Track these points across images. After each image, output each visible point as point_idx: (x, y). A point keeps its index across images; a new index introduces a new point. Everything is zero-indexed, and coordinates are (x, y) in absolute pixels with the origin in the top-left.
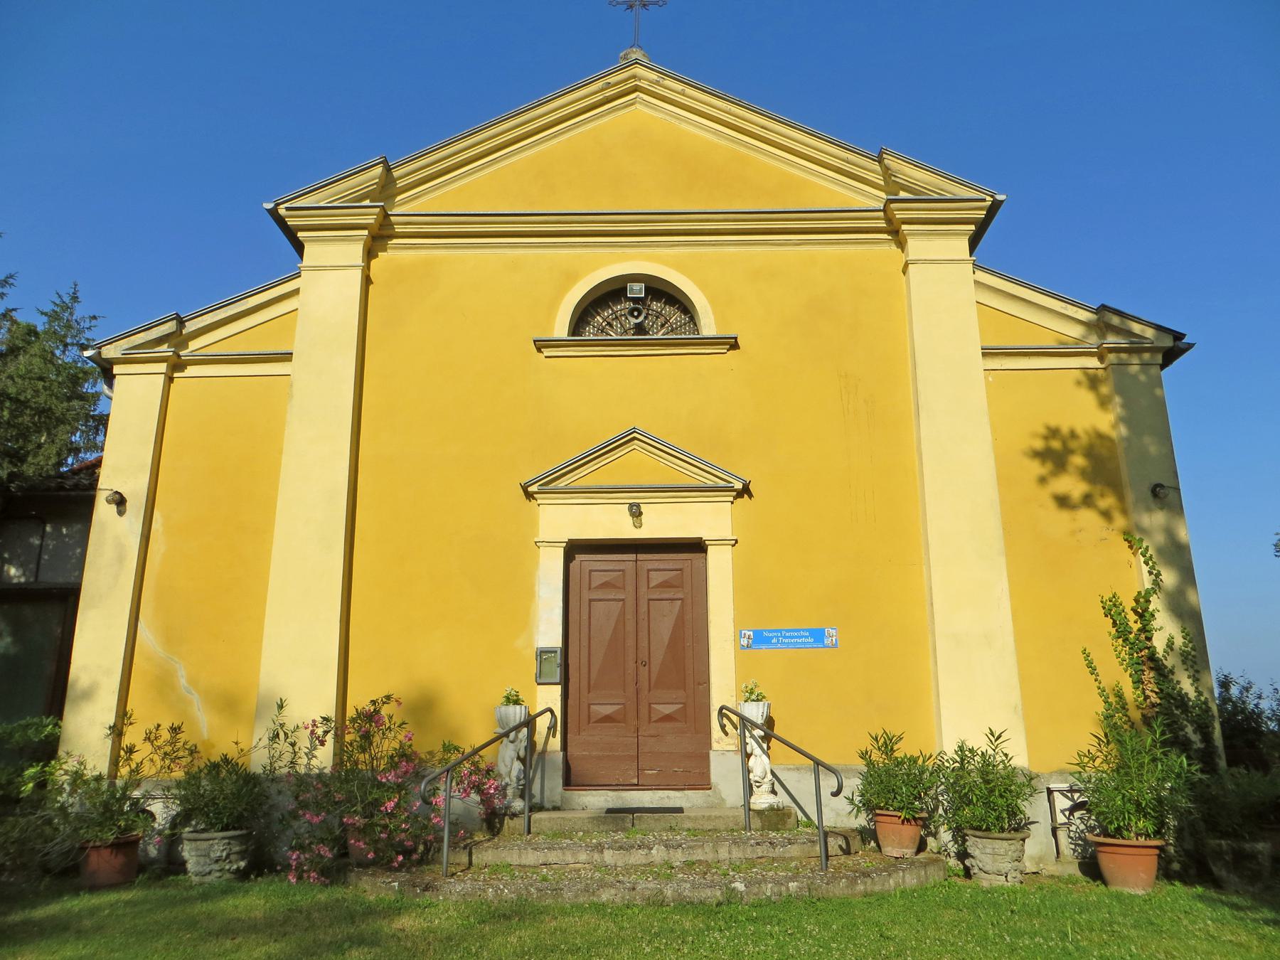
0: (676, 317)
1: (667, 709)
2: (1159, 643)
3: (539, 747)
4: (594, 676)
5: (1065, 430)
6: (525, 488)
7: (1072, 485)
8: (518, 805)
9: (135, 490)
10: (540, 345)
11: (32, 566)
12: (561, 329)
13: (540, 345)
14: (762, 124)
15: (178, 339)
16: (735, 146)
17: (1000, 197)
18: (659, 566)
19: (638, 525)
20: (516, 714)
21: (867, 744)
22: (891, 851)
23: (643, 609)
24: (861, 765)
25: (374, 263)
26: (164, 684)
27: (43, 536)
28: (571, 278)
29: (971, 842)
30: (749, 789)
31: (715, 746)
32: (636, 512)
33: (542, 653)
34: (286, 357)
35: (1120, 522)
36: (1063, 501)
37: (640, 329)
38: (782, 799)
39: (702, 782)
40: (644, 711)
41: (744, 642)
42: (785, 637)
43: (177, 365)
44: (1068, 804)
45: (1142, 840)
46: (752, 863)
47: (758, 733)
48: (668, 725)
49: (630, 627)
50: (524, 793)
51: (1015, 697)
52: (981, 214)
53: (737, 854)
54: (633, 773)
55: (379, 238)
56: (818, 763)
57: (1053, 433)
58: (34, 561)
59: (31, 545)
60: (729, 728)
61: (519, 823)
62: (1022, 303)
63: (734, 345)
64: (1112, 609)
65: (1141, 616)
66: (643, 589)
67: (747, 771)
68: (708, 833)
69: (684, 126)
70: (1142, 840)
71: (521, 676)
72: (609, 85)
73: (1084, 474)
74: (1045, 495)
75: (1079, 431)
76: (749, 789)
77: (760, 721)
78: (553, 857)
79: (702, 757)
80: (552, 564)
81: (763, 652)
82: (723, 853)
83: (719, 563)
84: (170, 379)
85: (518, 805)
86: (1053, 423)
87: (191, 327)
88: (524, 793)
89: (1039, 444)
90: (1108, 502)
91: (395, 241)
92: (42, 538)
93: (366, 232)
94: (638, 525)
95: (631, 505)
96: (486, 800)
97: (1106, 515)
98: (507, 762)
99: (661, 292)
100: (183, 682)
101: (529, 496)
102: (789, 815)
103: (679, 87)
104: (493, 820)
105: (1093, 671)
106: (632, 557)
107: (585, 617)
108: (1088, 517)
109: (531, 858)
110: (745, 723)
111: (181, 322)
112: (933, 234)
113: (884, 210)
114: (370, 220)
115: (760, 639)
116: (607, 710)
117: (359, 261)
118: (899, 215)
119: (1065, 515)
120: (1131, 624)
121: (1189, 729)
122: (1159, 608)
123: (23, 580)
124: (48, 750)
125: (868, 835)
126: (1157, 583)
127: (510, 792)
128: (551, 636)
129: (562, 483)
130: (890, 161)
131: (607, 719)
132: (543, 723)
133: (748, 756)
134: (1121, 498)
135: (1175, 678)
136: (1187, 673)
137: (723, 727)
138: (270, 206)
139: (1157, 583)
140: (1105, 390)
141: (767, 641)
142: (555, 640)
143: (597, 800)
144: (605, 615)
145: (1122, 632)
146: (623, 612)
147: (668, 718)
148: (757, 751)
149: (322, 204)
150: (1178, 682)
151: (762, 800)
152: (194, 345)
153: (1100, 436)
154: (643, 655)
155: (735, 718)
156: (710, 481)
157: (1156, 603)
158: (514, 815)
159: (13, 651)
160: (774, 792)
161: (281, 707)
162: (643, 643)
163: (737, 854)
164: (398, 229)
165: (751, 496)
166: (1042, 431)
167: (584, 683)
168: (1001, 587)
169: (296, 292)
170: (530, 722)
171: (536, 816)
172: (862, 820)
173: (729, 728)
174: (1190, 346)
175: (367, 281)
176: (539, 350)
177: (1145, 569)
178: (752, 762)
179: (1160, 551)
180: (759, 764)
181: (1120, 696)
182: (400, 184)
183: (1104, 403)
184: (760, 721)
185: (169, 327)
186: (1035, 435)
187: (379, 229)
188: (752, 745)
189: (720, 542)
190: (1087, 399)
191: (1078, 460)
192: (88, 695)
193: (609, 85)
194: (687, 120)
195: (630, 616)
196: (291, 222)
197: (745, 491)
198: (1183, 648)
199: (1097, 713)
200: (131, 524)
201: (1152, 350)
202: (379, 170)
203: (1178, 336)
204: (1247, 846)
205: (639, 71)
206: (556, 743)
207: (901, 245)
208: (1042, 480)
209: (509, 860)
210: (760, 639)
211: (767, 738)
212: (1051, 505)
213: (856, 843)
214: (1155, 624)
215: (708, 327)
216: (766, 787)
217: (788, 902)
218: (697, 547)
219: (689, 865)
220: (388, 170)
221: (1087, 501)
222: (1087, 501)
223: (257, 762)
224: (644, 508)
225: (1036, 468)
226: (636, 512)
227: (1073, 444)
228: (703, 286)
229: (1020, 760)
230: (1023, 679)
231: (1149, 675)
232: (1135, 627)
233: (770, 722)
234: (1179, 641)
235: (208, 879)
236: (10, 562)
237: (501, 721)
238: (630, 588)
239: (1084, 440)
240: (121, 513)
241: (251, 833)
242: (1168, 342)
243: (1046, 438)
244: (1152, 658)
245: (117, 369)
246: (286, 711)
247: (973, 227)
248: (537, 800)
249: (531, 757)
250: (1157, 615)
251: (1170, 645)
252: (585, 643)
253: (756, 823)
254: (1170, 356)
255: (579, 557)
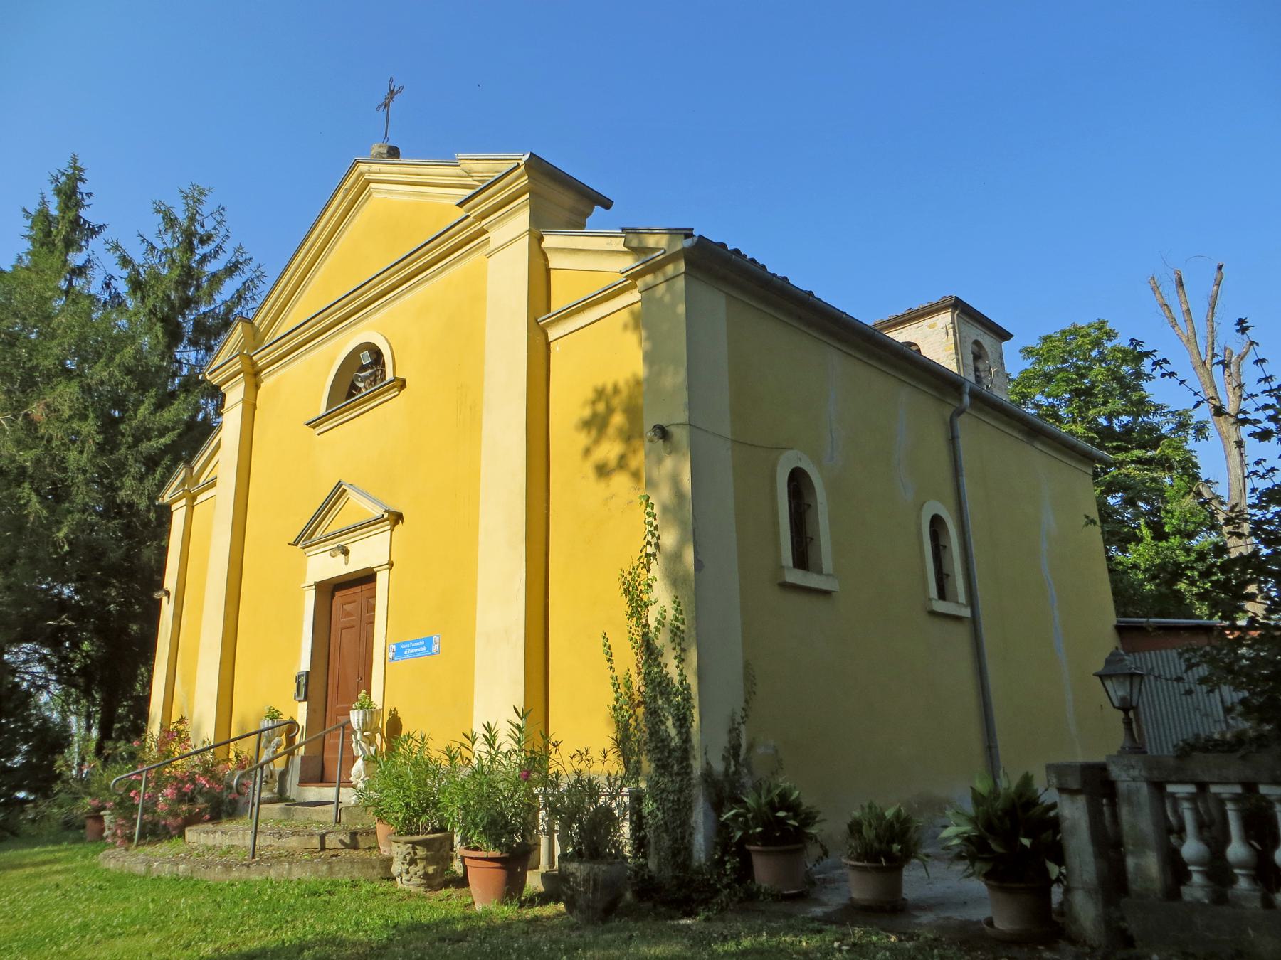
14: (398, 171)
42: (412, 648)
62: (583, 253)
72: (348, 191)
75: (622, 384)
91: (264, 373)
93: (242, 375)
112: (504, 218)
114: (239, 366)
115: (399, 652)
122: (657, 577)
128: (305, 666)
129: (318, 535)
136: (674, 653)
149: (226, 359)
150: (666, 665)
179: (665, 509)
181: (628, 681)
182: (262, 329)
187: (253, 368)
193: (348, 191)
194: (390, 192)
198: (674, 622)
199: (608, 706)
208: (587, 452)
221: (622, 463)
224: (350, 547)
234: (671, 614)
241: (9, 790)
247: (527, 195)
250: (655, 585)
255: (338, 594)
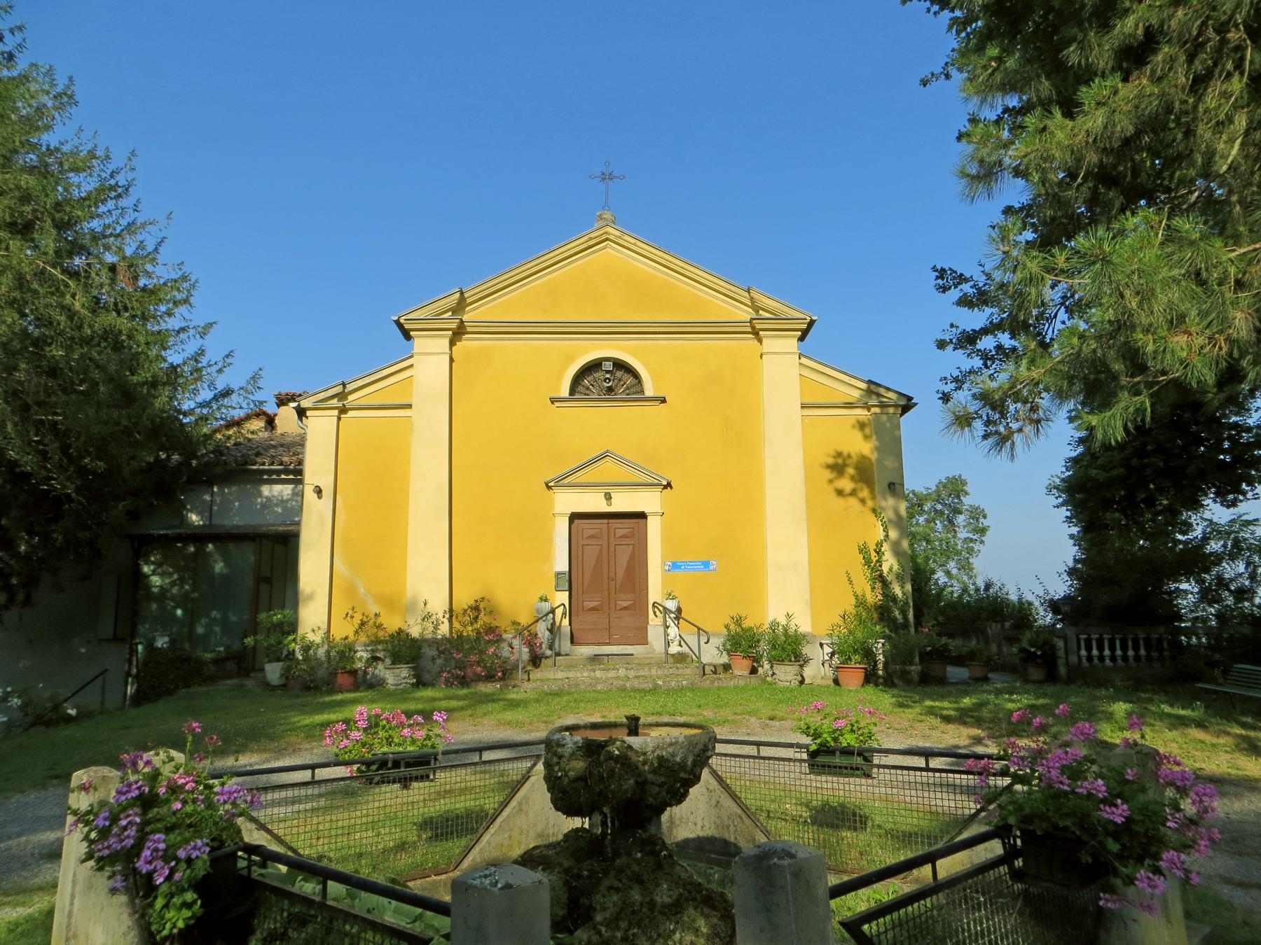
0: (630, 380)
1: (625, 604)
2: (885, 568)
3: (557, 624)
4: (585, 585)
5: (845, 453)
6: (547, 485)
7: (846, 484)
8: (548, 652)
9: (327, 484)
10: (553, 401)
11: (206, 514)
12: (565, 392)
13: (553, 401)
15: (342, 396)
16: (666, 277)
17: (814, 318)
18: (622, 527)
19: (610, 504)
20: (546, 606)
21: (728, 621)
22: (737, 672)
23: (612, 549)
24: (725, 631)
25: (454, 348)
26: (351, 591)
27: (212, 494)
28: (570, 359)
29: (775, 666)
30: (668, 644)
31: (650, 622)
32: (608, 497)
33: (558, 574)
34: (409, 406)
35: (870, 503)
36: (840, 493)
37: (610, 390)
38: (685, 649)
39: (644, 641)
40: (612, 604)
41: (667, 568)
43: (343, 410)
44: (831, 650)
45: (857, 666)
46: (667, 676)
47: (673, 616)
48: (625, 612)
49: (605, 560)
50: (551, 647)
51: (807, 596)
52: (805, 326)
53: (660, 672)
54: (607, 637)
55: (458, 334)
56: (699, 629)
57: (839, 454)
58: (207, 511)
59: (206, 500)
60: (658, 613)
61: (550, 661)
63: (664, 401)
64: (863, 550)
65: (878, 553)
66: (612, 540)
67: (666, 635)
68: (646, 663)
69: (635, 263)
70: (857, 666)
71: (548, 586)
72: (593, 235)
73: (852, 478)
74: (831, 489)
75: (853, 454)
76: (668, 644)
77: (674, 610)
78: (570, 675)
79: (643, 629)
80: (562, 526)
81: (677, 573)
82: (653, 672)
83: (654, 525)
84: (339, 418)
85: (548, 652)
86: (839, 448)
87: (349, 388)
88: (551, 647)
89: (831, 461)
90: (865, 493)
92: (212, 496)
94: (610, 504)
95: (606, 494)
96: (532, 651)
97: (863, 501)
98: (542, 629)
99: (620, 365)
100: (362, 590)
101: (549, 488)
102: (688, 657)
103: (633, 241)
104: (536, 660)
105: (851, 582)
106: (606, 521)
107: (580, 555)
108: (853, 501)
109: (560, 675)
110: (666, 611)
111: (344, 385)
113: (750, 322)
115: (675, 566)
116: (593, 604)
117: (447, 350)
118: (758, 326)
119: (841, 502)
120: (873, 558)
121: (897, 613)
123: (201, 523)
124: (291, 626)
125: (727, 667)
126: (887, 536)
127: (544, 646)
129: (566, 481)
130: (753, 294)
131: (593, 609)
132: (559, 612)
133: (668, 627)
134: (872, 491)
135: (892, 586)
137: (655, 613)
138: (396, 318)
139: (887, 536)
140: (867, 431)
141: (679, 567)
142: (564, 567)
143: (586, 651)
144: (591, 555)
145: (868, 562)
146: (601, 549)
147: (625, 608)
148: (672, 625)
151: (674, 649)
152: (351, 398)
153: (864, 457)
154: (612, 575)
155: (661, 608)
156: (650, 480)
157: (886, 547)
158: (547, 658)
159: (225, 571)
160: (680, 645)
161: (425, 604)
162: (612, 569)
163: (660, 672)
164: (469, 329)
165: (671, 488)
166: (833, 453)
167: (580, 590)
168: (803, 540)
169: (412, 366)
170: (553, 611)
171: (558, 658)
172: (724, 659)
173: (658, 613)
174: (916, 404)
175: (452, 360)
176: (552, 403)
177: (882, 528)
178: (669, 630)
180: (673, 631)
182: (469, 301)
183: (866, 437)
184: (674, 610)
185: (339, 389)
186: (828, 455)
188: (669, 622)
189: (655, 514)
190: (858, 435)
191: (851, 471)
192: (310, 597)
195: (605, 550)
196: (407, 327)
197: (669, 485)
200: (326, 504)
201: (896, 406)
202: (458, 295)
203: (910, 399)
204: (907, 668)
205: (609, 229)
206: (566, 622)
207: (760, 341)
208: (831, 481)
209: (549, 677)
210: (675, 566)
211: (678, 618)
212: (834, 494)
213: (720, 670)
214: (884, 558)
215: (649, 391)
216: (676, 643)
217: (682, 689)
218: (642, 516)
219: (638, 677)
220: (462, 293)
221: (853, 493)
222: (853, 493)
223: (415, 632)
224: (612, 495)
225: (828, 474)
226: (608, 497)
227: (848, 462)
228: (646, 364)
229: (802, 630)
230: (812, 590)
231: (878, 585)
232: (874, 560)
233: (679, 610)
234: (896, 567)
235: (401, 687)
236: (191, 511)
237: (538, 611)
238: (605, 538)
239: (855, 459)
240: (320, 497)
242: (903, 402)
243: (835, 457)
244: (881, 576)
245: (308, 413)
246: (428, 606)
247: (800, 333)
248: (557, 650)
249: (553, 629)
251: (891, 569)
252: (580, 568)
253: (671, 660)
254: (906, 409)
